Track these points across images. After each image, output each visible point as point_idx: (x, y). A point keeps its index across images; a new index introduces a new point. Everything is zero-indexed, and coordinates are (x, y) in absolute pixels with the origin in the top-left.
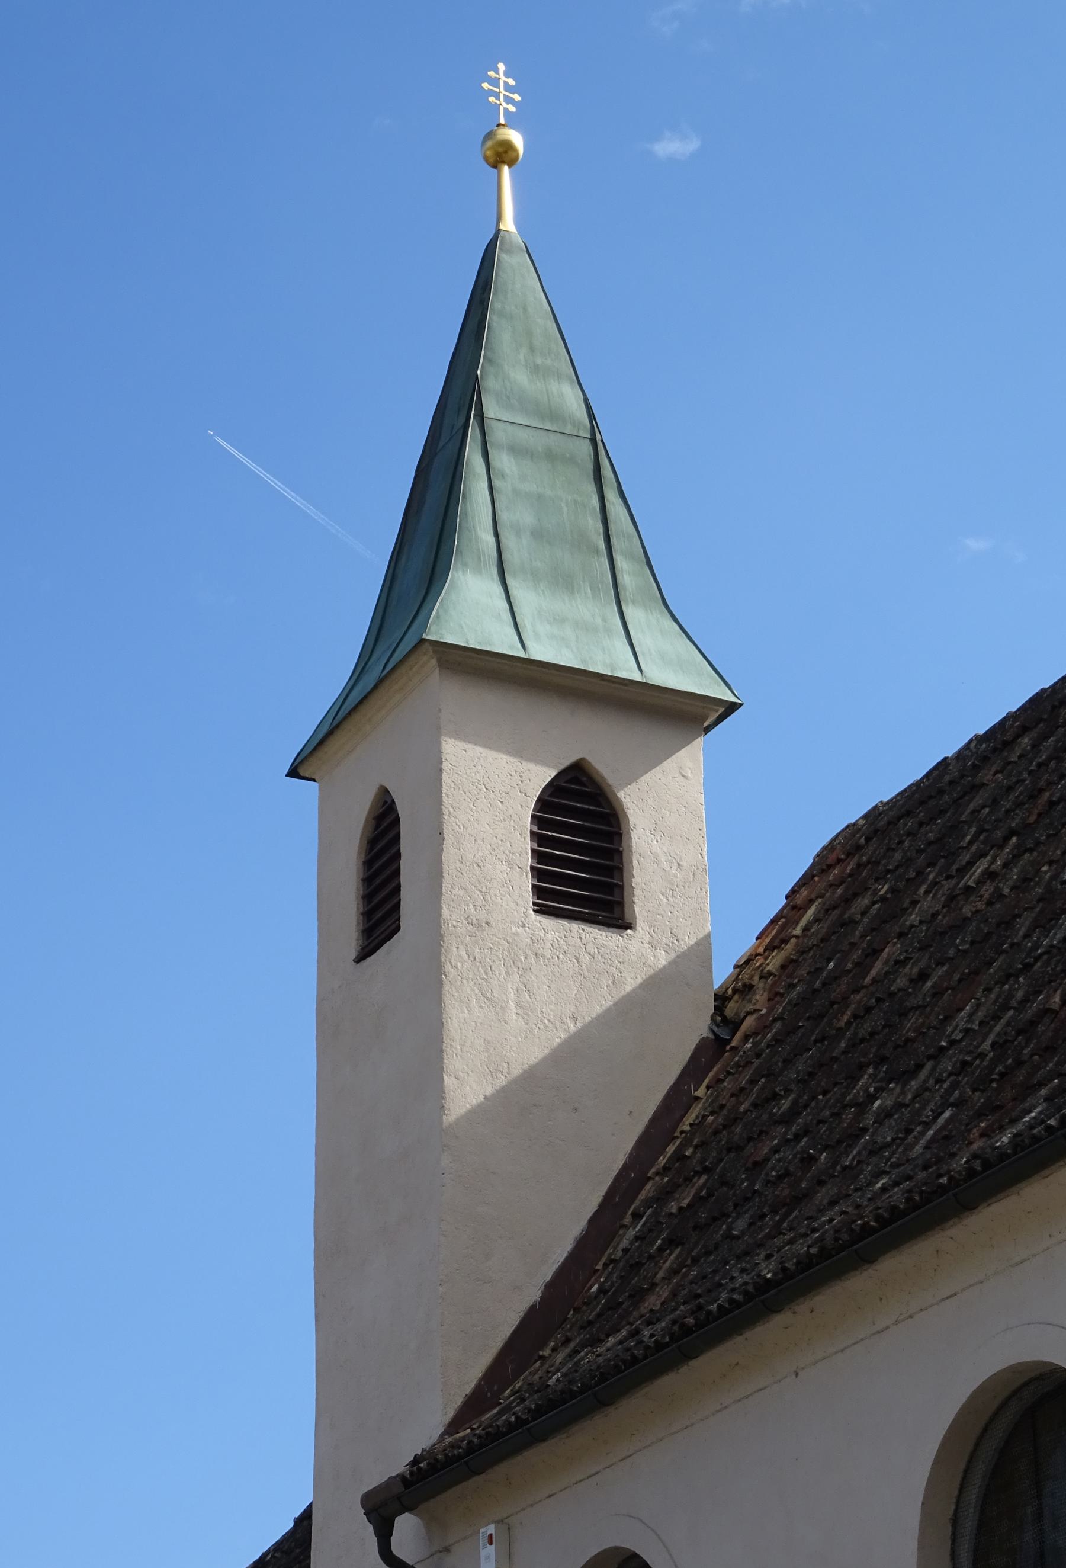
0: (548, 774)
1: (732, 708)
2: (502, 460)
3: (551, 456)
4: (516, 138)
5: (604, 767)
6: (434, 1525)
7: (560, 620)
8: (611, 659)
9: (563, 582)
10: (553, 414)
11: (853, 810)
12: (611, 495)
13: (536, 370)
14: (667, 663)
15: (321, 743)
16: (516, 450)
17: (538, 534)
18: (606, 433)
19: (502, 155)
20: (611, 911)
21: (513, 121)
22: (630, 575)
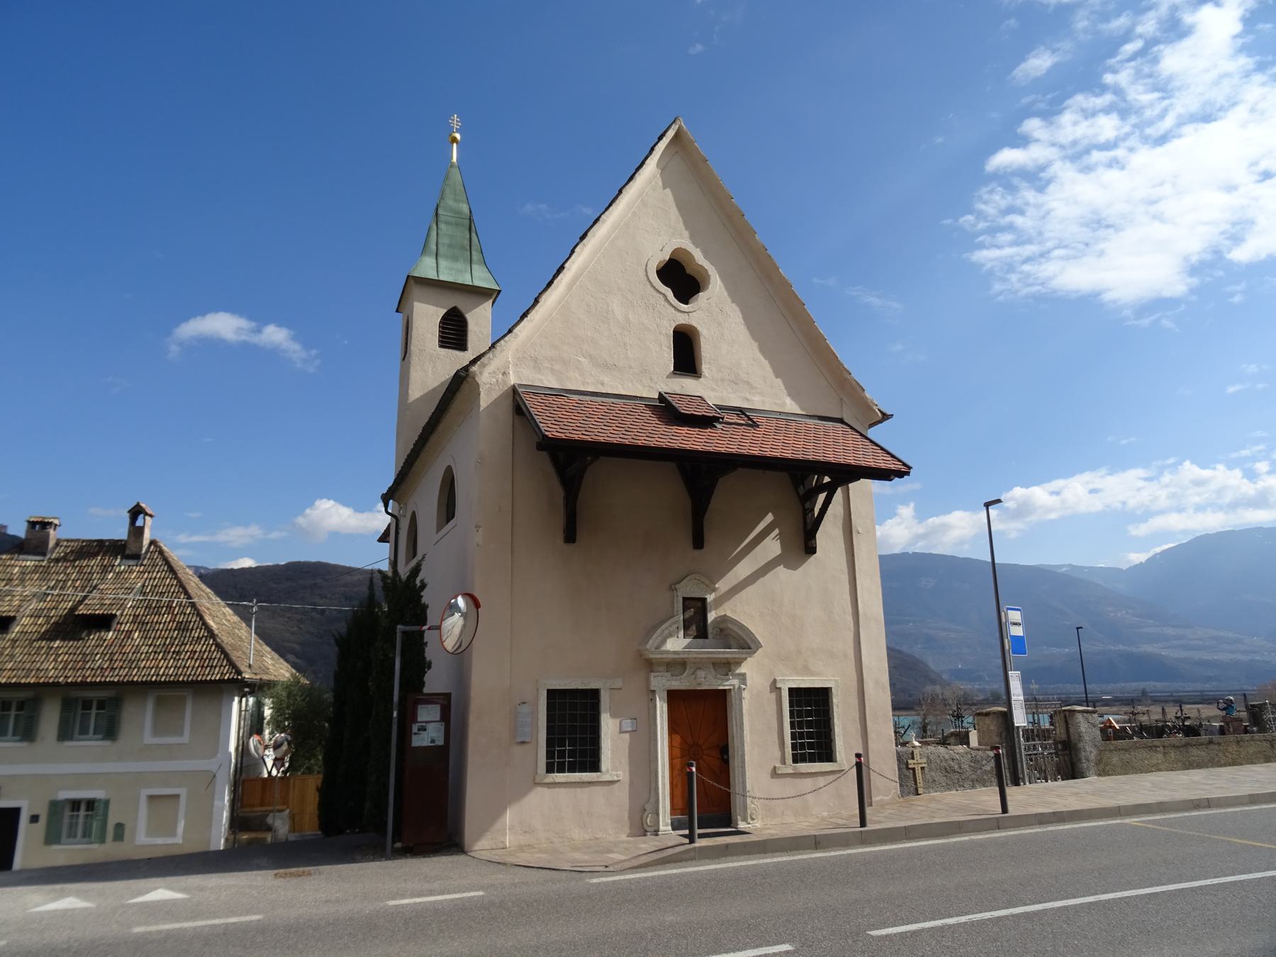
0: (443, 311)
1: (499, 292)
2: (442, 226)
3: (457, 224)
4: (458, 136)
5: (461, 308)
6: (398, 501)
7: (451, 269)
8: (465, 279)
9: (455, 258)
10: (459, 212)
11: (302, 559)
12: (474, 234)
13: (456, 200)
14: (481, 278)
15: (407, 328)
16: (447, 223)
17: (450, 246)
18: (475, 217)
19: (454, 140)
20: (1262, 707)
21: (458, 131)
22: (476, 255)
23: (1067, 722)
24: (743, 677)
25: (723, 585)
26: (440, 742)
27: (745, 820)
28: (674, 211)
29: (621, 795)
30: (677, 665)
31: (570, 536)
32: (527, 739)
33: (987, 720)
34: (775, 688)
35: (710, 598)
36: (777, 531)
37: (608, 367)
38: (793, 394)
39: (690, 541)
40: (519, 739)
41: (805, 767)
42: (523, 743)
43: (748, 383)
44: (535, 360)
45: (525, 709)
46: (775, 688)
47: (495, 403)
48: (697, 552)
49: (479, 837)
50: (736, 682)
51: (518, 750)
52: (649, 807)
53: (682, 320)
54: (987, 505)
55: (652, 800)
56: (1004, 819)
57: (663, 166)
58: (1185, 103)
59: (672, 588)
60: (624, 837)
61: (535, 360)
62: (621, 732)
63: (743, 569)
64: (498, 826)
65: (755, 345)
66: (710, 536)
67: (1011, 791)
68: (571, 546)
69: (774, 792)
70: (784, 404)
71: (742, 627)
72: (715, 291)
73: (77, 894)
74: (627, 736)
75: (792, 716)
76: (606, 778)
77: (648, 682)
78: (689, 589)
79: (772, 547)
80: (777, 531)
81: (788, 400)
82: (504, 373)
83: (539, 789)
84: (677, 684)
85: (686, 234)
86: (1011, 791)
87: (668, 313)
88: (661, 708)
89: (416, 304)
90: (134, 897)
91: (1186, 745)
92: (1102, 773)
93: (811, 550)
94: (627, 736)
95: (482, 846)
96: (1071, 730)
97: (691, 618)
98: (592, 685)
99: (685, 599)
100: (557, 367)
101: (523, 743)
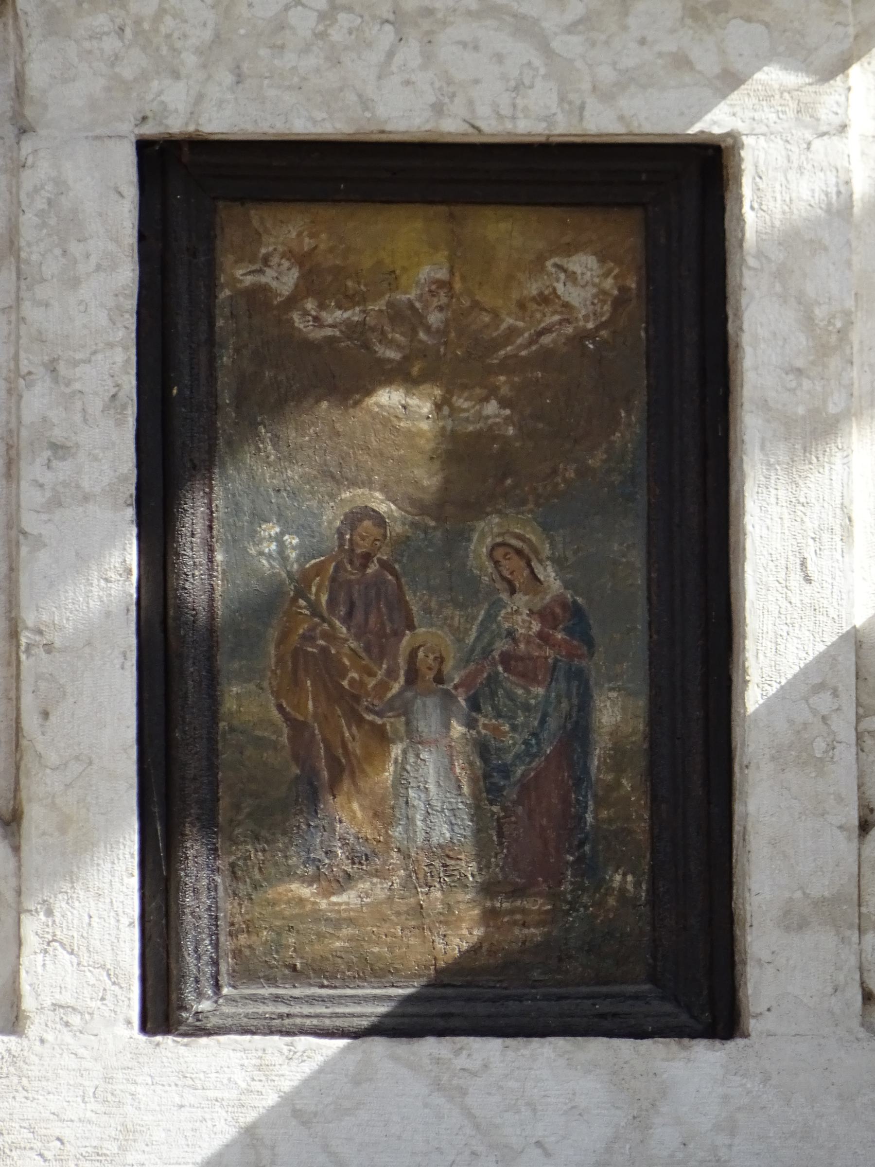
38: (770, 705)
66: (848, 662)
97: (365, 583)
99: (191, 188)
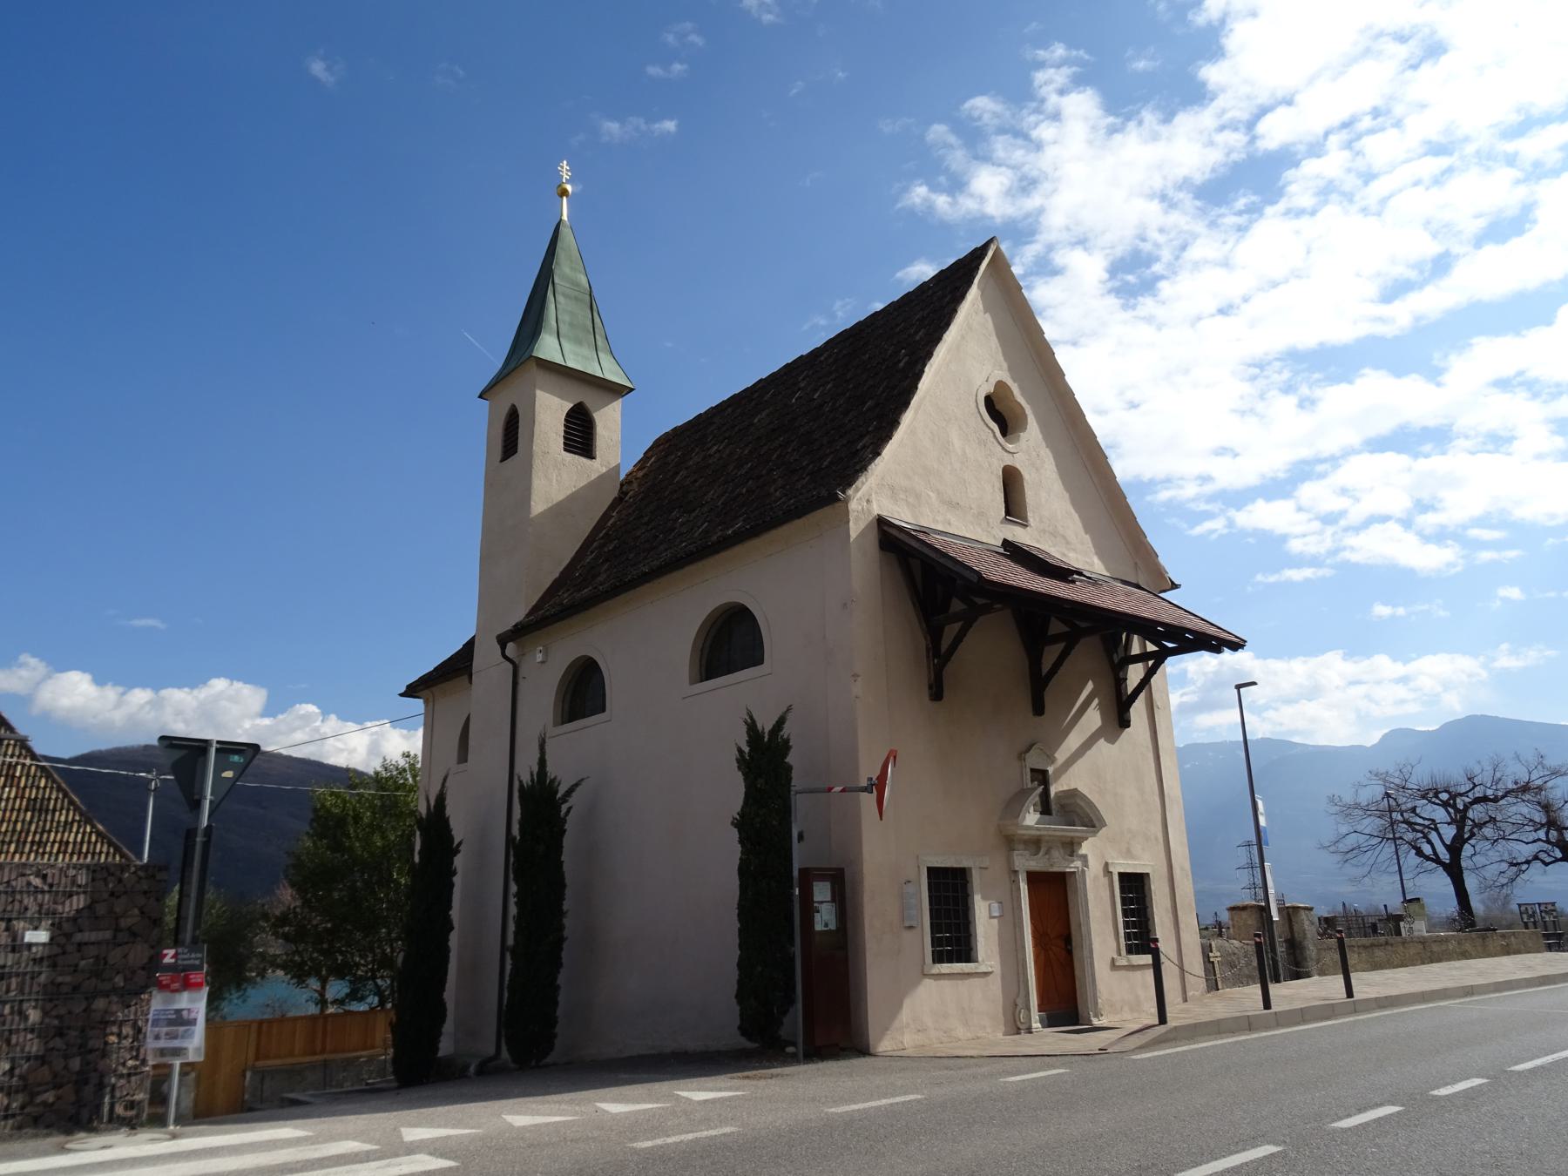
2: (560, 298)
3: (576, 299)
4: (569, 188)
5: (589, 404)
10: (578, 284)
16: (564, 295)
17: (571, 325)
18: (595, 293)
19: (564, 193)
23: (1290, 921)
24: (1084, 858)
25: (1062, 755)
26: (832, 926)
27: (1096, 1016)
28: (994, 340)
29: (995, 986)
30: (1035, 844)
31: (936, 693)
32: (914, 923)
33: (1244, 915)
34: (1107, 872)
35: (1051, 770)
36: (1096, 701)
37: (953, 505)
38: (1100, 553)
39: (1030, 708)
40: (907, 924)
41: (945, 968)
42: (911, 927)
43: (1064, 537)
44: (892, 488)
45: (910, 889)
46: (1107, 872)
47: (862, 534)
48: (1037, 719)
49: (880, 1039)
50: (1078, 863)
51: (907, 935)
52: (1020, 1001)
53: (1008, 460)
54: (1238, 687)
55: (1022, 993)
56: (1269, 1015)
57: (982, 289)
58: (1166, 255)
59: (1021, 756)
60: (1000, 1035)
61: (892, 488)
62: (991, 917)
63: (1073, 741)
64: (896, 1024)
65: (1067, 495)
67: (1274, 989)
68: (936, 704)
69: (1117, 988)
70: (1092, 565)
71: (1090, 803)
72: (1032, 434)
73: (296, 1127)
74: (995, 921)
75: (1123, 903)
76: (983, 969)
77: (1010, 861)
78: (1034, 760)
79: (1093, 718)
80: (1096, 701)
81: (1096, 560)
82: (868, 501)
83: (927, 982)
84: (1037, 864)
85: (1005, 365)
86: (1274, 989)
87: (990, 453)
88: (1024, 887)
89: (539, 393)
90: (730, 1099)
91: (1372, 945)
92: (1322, 973)
93: (1124, 723)
94: (995, 921)
95: (885, 1046)
96: (1296, 928)
98: (964, 863)
100: (911, 500)
101: (911, 927)
